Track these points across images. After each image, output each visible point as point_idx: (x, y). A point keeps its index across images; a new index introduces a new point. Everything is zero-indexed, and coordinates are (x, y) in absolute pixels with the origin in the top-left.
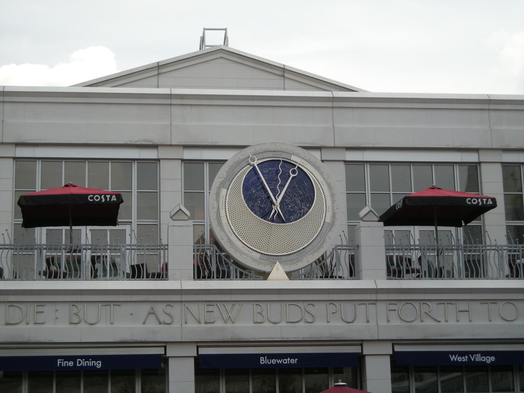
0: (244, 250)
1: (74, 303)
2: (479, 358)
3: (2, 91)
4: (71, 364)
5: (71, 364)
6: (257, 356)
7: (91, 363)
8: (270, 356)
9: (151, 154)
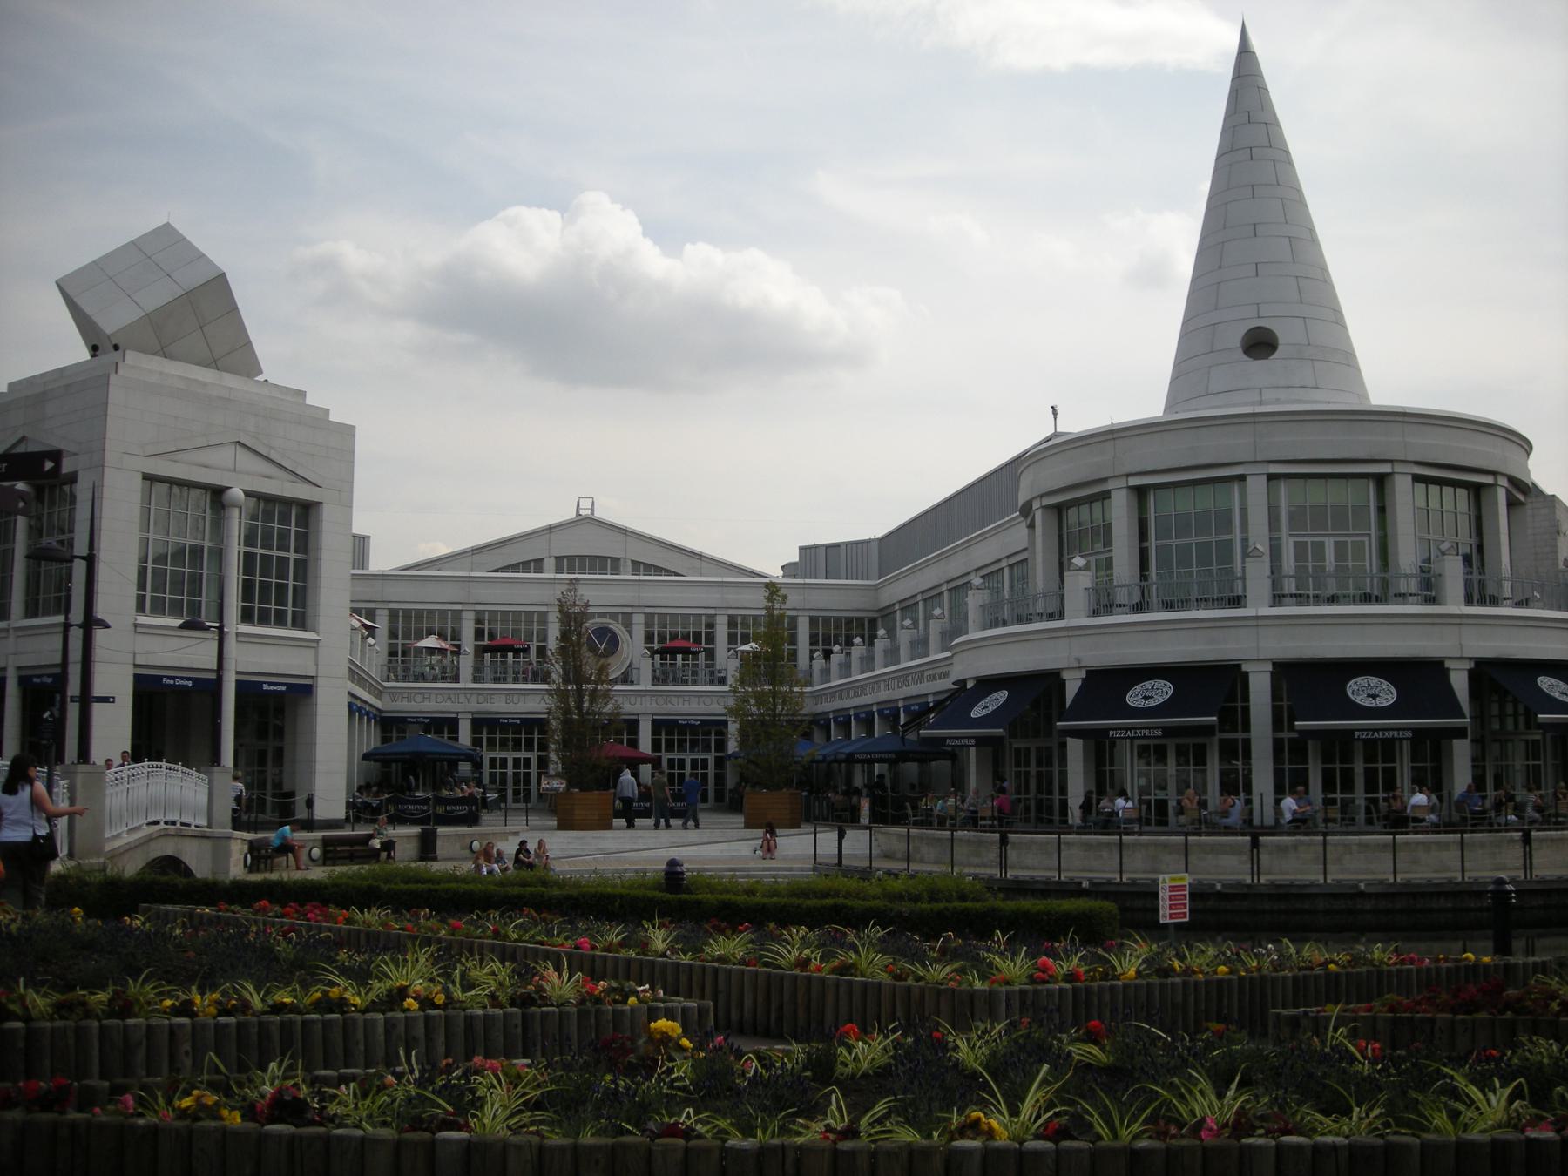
0: (939, 671)
1: (699, 696)
2: (693, 722)
3: (81, 630)
4: (172, 682)
5: (172, 682)
6: (161, 677)
7: (185, 683)
8: (271, 684)
9: (544, 609)
